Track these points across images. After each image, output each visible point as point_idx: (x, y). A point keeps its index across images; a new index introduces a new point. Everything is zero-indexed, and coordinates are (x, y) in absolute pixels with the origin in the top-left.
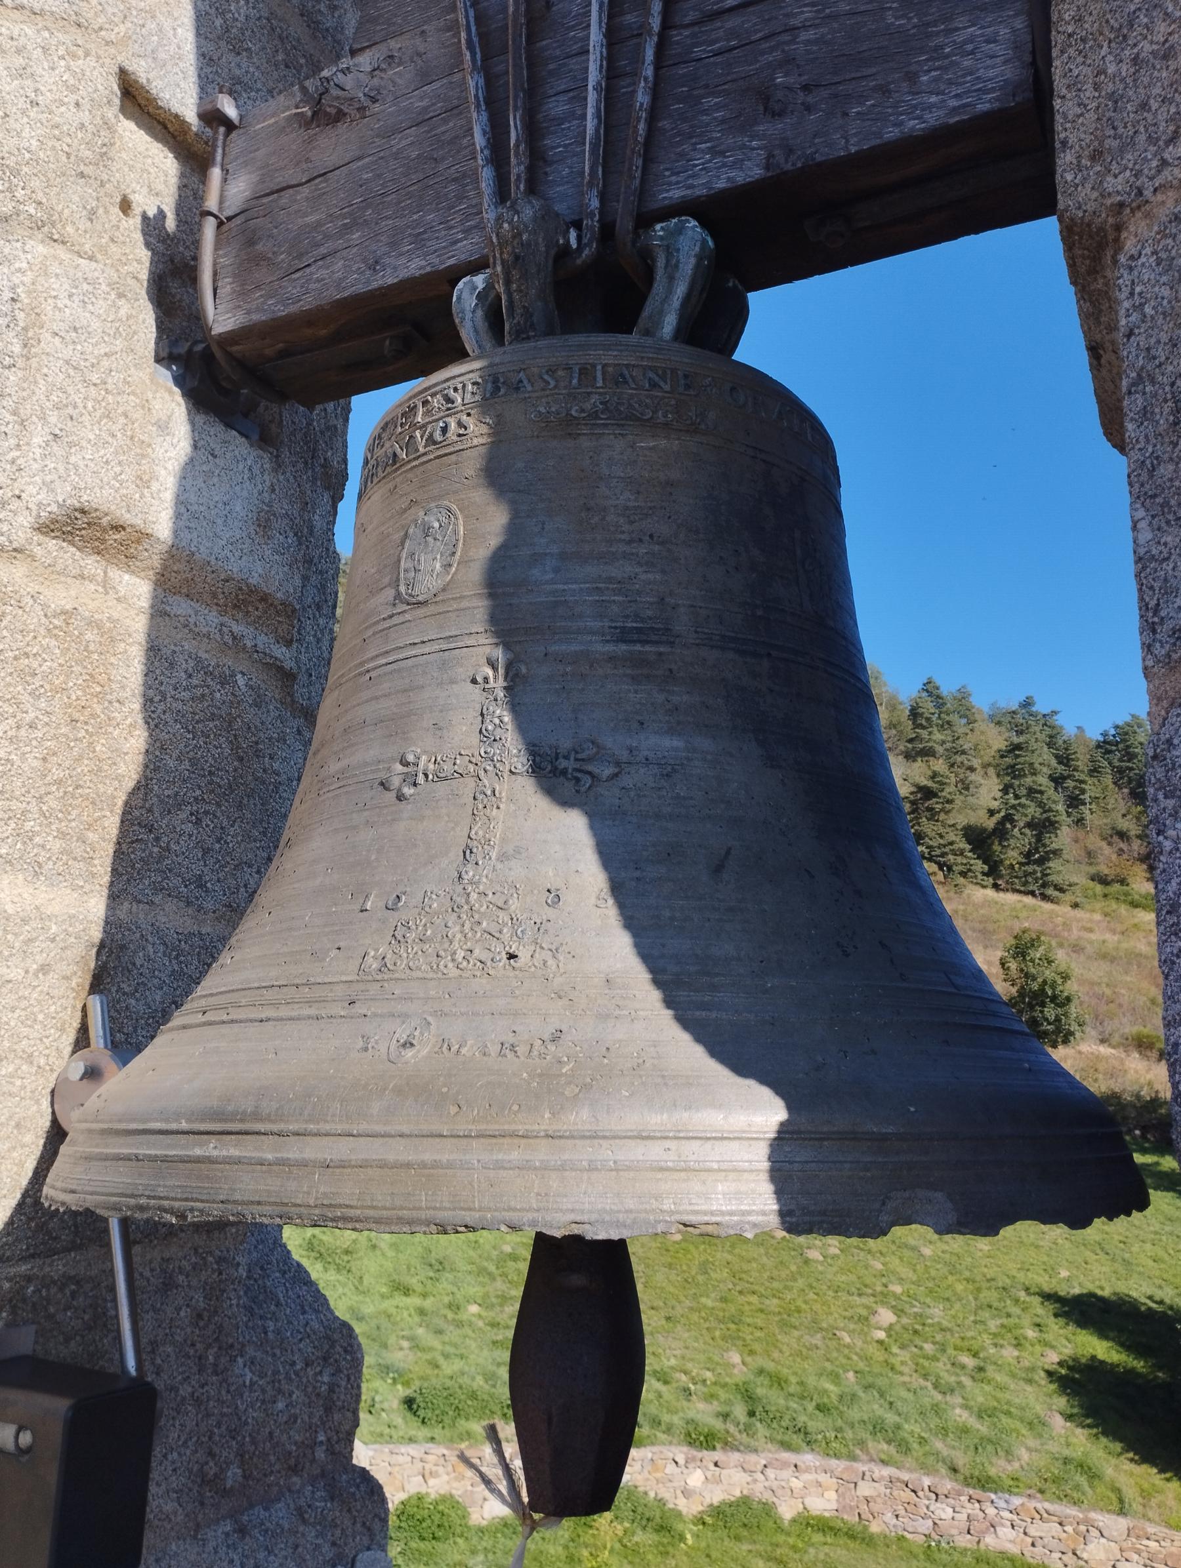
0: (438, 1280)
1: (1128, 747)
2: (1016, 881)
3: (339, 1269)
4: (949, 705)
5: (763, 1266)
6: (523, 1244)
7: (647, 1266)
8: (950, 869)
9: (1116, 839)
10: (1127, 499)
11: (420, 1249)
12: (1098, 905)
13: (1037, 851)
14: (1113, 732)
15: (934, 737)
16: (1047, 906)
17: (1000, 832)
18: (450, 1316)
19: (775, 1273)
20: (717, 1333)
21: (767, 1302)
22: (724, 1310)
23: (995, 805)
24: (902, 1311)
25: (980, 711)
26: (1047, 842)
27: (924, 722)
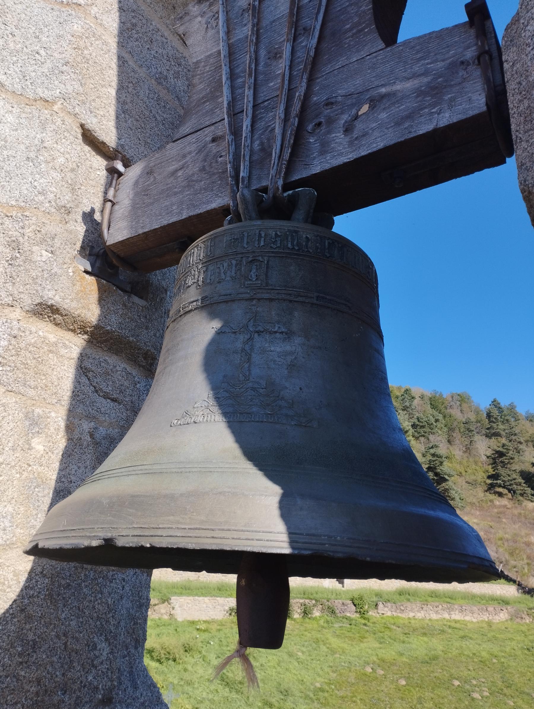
0: (286, 701)
3: (237, 692)
4: (505, 412)
5: (451, 701)
6: (326, 683)
7: (390, 698)
8: (514, 492)
11: (275, 683)
15: (499, 427)
27: (494, 420)
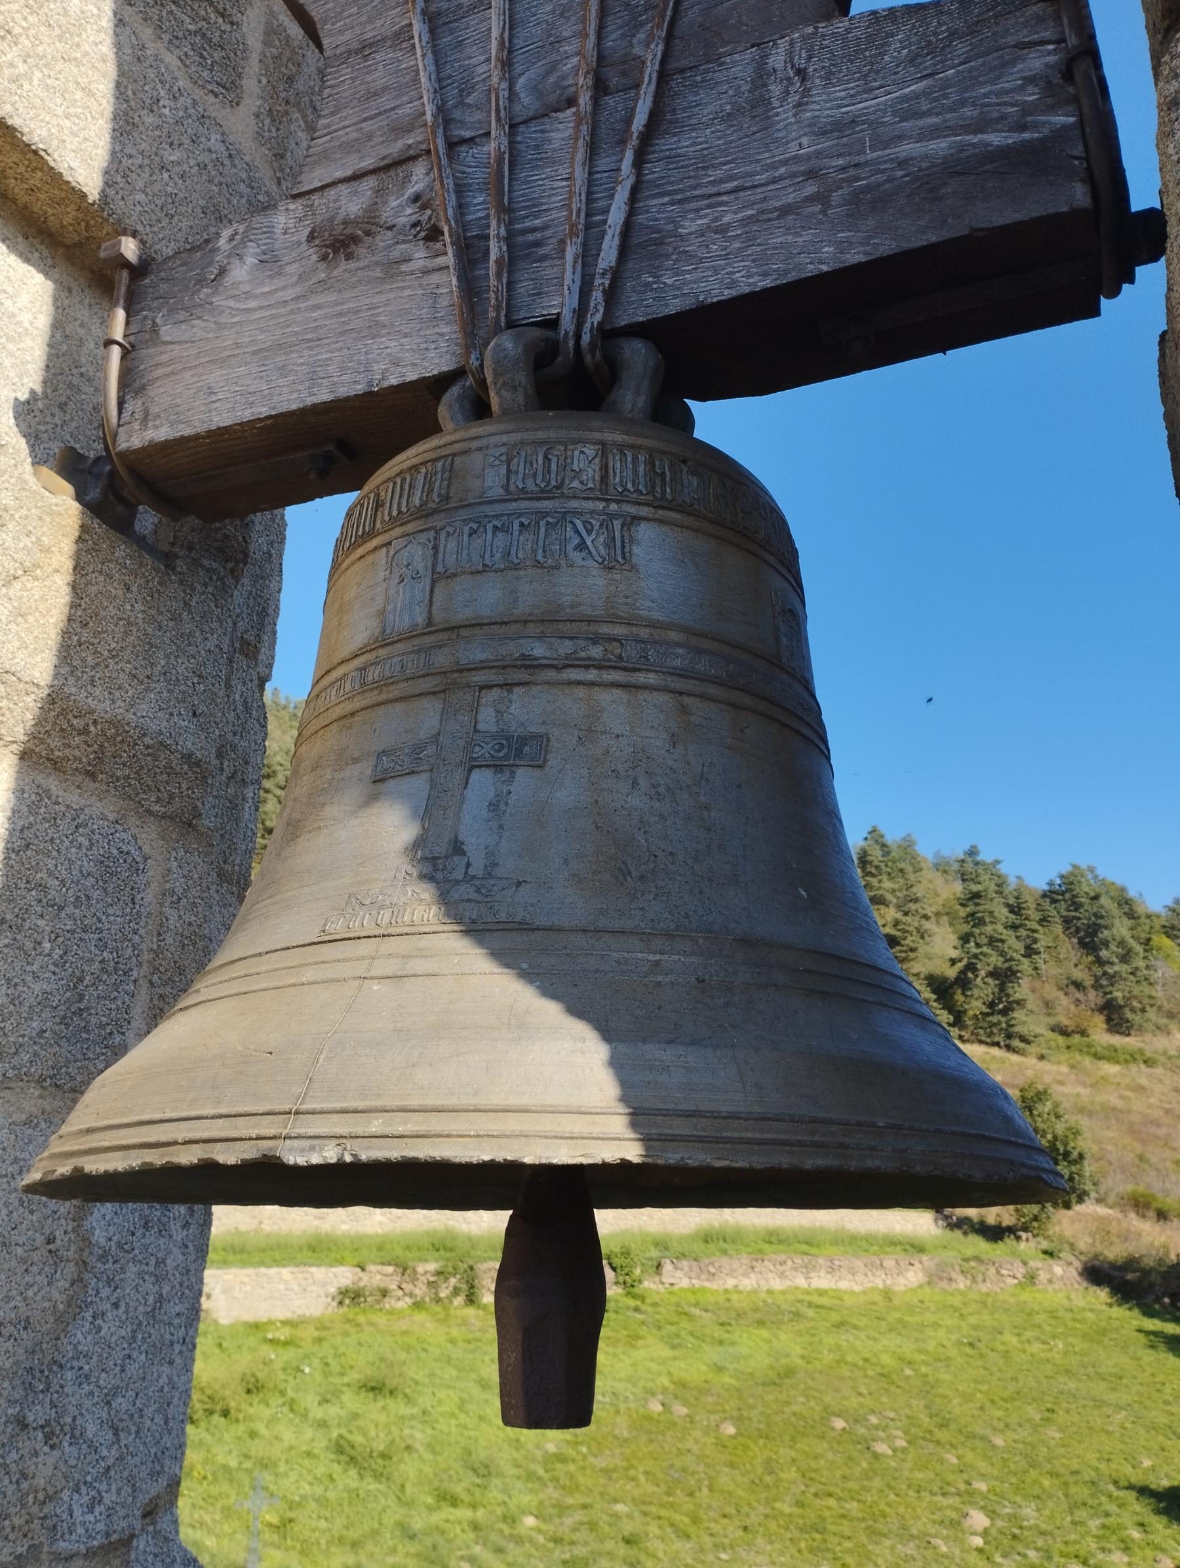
0: (486, 1488)
1: (1076, 896)
2: (981, 1031)
4: (893, 854)
9: (1072, 988)
10: (279, 623)
12: (1063, 1057)
13: (1000, 999)
14: (1058, 881)
16: (1015, 1058)
17: (963, 982)
18: (507, 1530)
19: (847, 1472)
20: (803, 1545)
21: (847, 1506)
22: (803, 1517)
23: (955, 954)
24: (994, 1512)
25: (925, 860)
26: (1010, 991)
27: (873, 870)
